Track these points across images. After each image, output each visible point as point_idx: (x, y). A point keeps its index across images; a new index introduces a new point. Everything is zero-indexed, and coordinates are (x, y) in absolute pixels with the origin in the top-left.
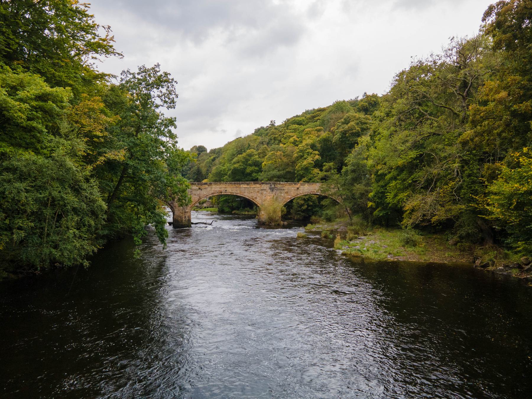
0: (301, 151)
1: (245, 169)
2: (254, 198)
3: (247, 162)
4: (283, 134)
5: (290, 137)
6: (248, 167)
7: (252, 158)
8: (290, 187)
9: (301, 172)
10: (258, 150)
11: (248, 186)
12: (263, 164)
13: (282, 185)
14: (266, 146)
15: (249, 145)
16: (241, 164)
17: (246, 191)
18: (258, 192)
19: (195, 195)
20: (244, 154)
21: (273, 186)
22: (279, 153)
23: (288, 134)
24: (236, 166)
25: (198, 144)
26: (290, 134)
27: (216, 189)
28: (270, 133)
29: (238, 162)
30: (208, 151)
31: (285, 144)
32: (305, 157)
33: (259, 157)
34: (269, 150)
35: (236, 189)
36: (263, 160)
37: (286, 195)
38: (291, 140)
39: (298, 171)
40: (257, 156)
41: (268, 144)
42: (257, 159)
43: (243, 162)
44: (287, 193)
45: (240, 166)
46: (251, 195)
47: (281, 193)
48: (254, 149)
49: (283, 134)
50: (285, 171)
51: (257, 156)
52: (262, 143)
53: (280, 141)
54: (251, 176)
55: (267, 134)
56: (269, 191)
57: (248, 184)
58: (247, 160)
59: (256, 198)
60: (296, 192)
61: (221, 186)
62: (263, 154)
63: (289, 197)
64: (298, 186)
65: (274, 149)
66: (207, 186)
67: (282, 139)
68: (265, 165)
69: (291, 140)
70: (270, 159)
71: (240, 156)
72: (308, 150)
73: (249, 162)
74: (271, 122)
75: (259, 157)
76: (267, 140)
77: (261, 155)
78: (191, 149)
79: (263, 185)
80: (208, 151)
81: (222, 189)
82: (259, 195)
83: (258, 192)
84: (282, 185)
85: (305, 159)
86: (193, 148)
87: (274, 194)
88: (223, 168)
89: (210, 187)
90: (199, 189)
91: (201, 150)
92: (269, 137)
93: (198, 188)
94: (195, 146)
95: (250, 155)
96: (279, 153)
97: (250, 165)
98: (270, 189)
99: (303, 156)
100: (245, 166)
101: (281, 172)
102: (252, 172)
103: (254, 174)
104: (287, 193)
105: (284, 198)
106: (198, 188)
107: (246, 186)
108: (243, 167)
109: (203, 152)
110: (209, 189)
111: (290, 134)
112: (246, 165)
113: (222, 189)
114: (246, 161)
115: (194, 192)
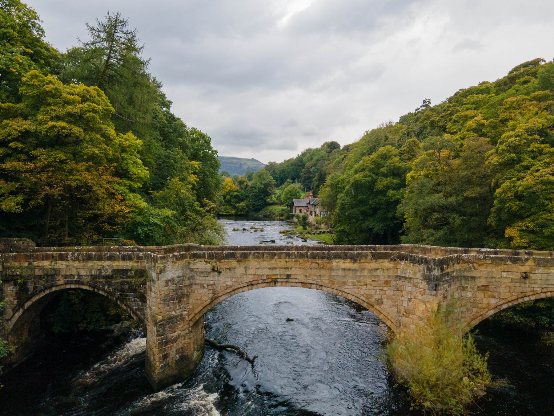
0: (514, 149)
1: (374, 182)
2: (372, 300)
3: (379, 168)
4: (450, 115)
5: (466, 118)
6: (380, 178)
7: (389, 161)
8: (496, 271)
9: (515, 206)
10: (400, 146)
11: (356, 266)
12: (408, 175)
13: (468, 262)
14: (414, 138)
15: (387, 138)
16: (367, 173)
17: (350, 279)
18: (387, 283)
19: (202, 286)
20: (374, 156)
21: (436, 272)
22: (445, 153)
23: (460, 114)
24: (358, 176)
25: (329, 140)
26: (467, 113)
27: (260, 272)
28: (423, 117)
29: (363, 170)
30: (341, 148)
31: (453, 133)
32: (525, 163)
33: (402, 160)
34: (421, 145)
35: (317, 272)
36: (409, 164)
37: (480, 295)
38: (471, 123)
39: (502, 201)
40: (397, 159)
41: (418, 135)
42: (398, 164)
43: (371, 170)
44: (484, 288)
45: (366, 176)
46: (364, 290)
47: (464, 288)
48: (392, 145)
49: (450, 115)
50: (460, 198)
51: (397, 159)
52: (408, 134)
53: (444, 129)
54: (385, 196)
55: (417, 120)
56: (424, 285)
57: (354, 259)
58: (379, 166)
59: (380, 302)
60: (519, 288)
61: (272, 264)
62: (411, 154)
63: (493, 301)
64: (526, 268)
65: (433, 146)
66: (233, 263)
67: (449, 125)
68: (413, 178)
69: (471, 123)
70: (422, 165)
71: (366, 158)
72: (533, 146)
73: (382, 169)
74: (424, 101)
75: (402, 160)
76: (417, 128)
77: (406, 156)
78: (322, 146)
79: (403, 264)
80: (341, 148)
81: (277, 272)
82: (390, 293)
83: (387, 283)
84: (468, 262)
85: (527, 168)
86: (324, 144)
87: (440, 297)
88: (342, 177)
89: (243, 265)
90: (213, 270)
91: (333, 146)
92: (421, 125)
93: (209, 266)
94: (326, 143)
95: (385, 157)
96: (445, 153)
97: (385, 175)
98: (428, 279)
99: (520, 160)
100: (375, 177)
101: (452, 200)
102: (388, 187)
103: (391, 192)
104: (484, 288)
105: (474, 303)
106: (209, 266)
107: (347, 264)
108: (370, 179)
109: (335, 150)
110: (240, 270)
111: (467, 113)
112: (377, 174)
113: (277, 272)
114: (376, 168)
115: (199, 279)
